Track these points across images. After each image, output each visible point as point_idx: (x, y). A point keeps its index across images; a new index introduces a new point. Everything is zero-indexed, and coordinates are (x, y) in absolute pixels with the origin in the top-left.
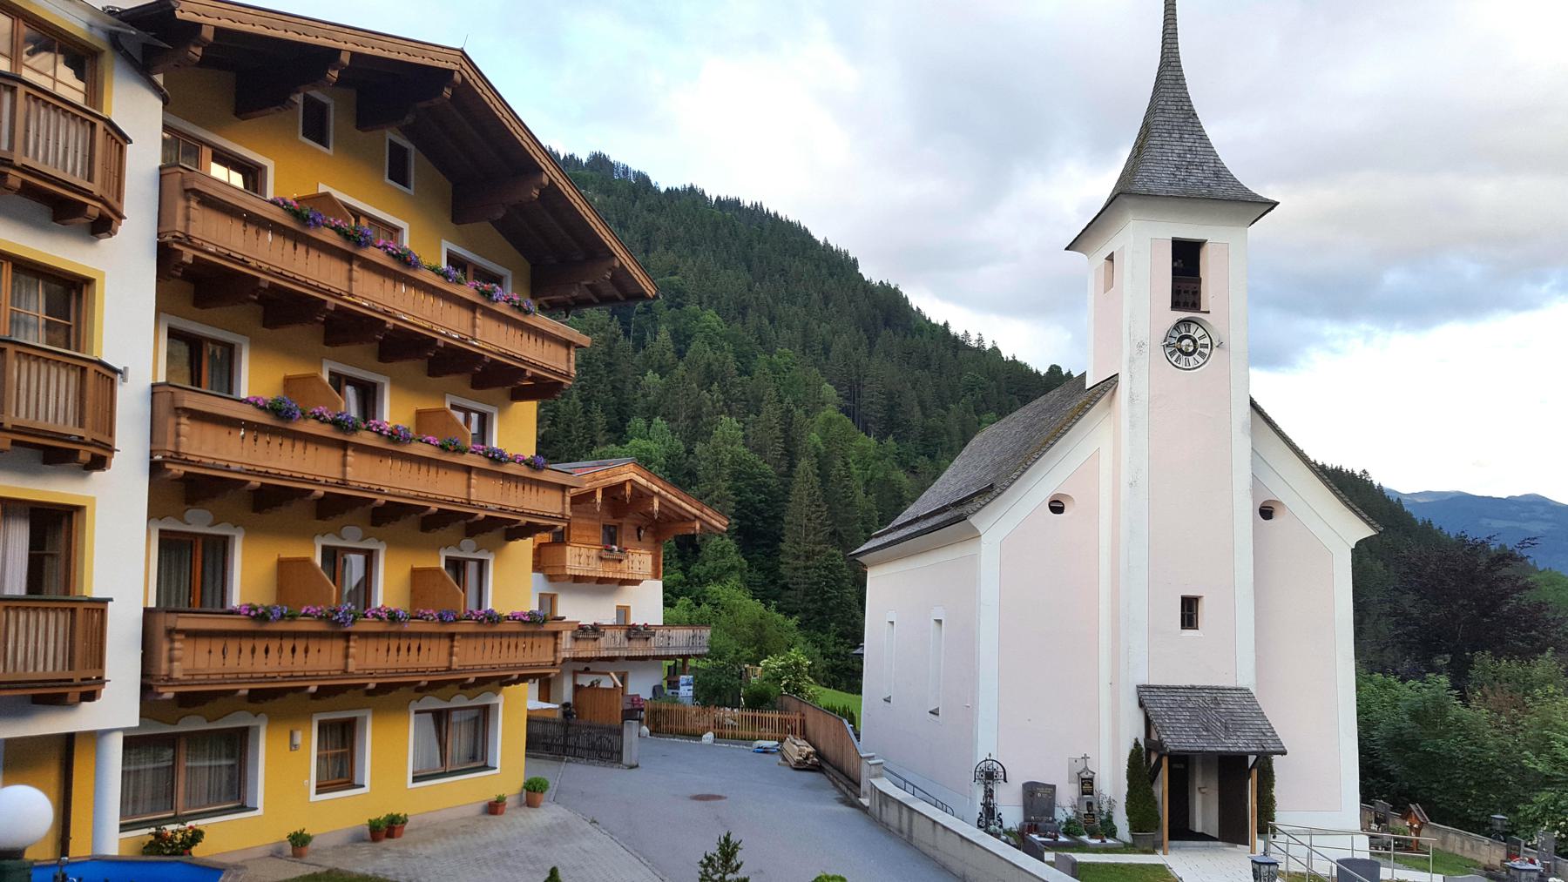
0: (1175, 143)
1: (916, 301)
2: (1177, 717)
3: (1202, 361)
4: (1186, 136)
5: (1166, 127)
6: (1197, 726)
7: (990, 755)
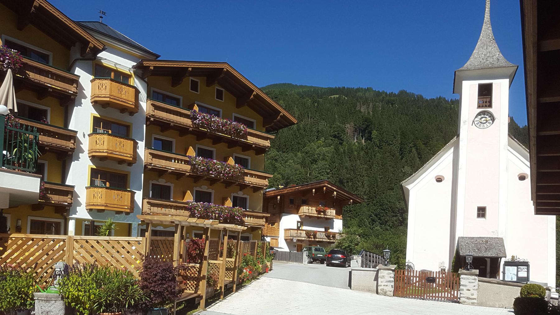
4: (489, 47)
7: (409, 261)
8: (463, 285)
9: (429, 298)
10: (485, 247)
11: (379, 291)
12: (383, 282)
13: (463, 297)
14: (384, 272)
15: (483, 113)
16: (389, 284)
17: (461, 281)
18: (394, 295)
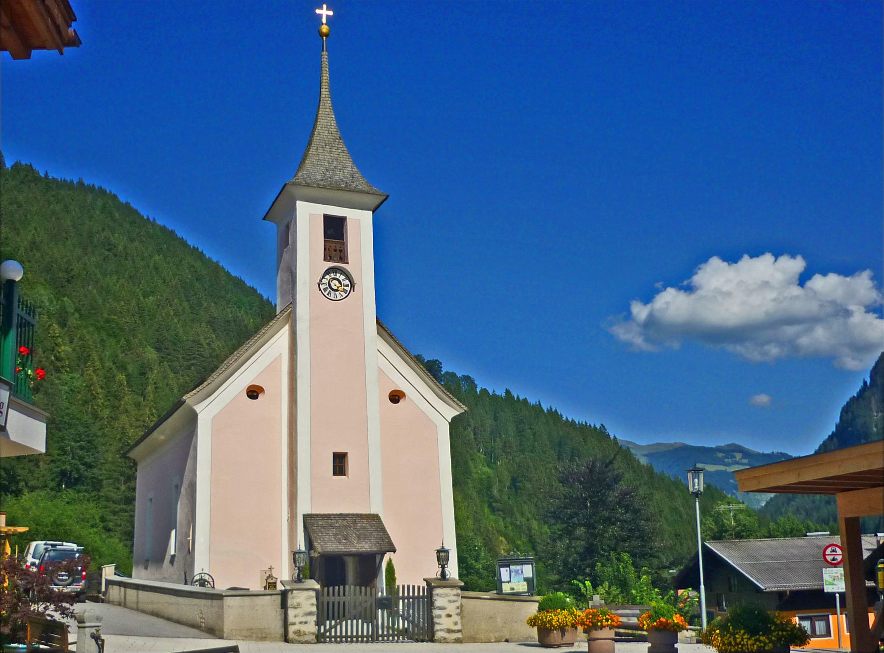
0: (327, 154)
1: (789, 454)
2: (327, 532)
3: (345, 295)
4: (335, 150)
5: (321, 144)
6: (340, 537)
7: (203, 570)
8: (440, 608)
9: (383, 640)
11: (291, 635)
12: (298, 616)
17: (435, 600)
18: (317, 640)
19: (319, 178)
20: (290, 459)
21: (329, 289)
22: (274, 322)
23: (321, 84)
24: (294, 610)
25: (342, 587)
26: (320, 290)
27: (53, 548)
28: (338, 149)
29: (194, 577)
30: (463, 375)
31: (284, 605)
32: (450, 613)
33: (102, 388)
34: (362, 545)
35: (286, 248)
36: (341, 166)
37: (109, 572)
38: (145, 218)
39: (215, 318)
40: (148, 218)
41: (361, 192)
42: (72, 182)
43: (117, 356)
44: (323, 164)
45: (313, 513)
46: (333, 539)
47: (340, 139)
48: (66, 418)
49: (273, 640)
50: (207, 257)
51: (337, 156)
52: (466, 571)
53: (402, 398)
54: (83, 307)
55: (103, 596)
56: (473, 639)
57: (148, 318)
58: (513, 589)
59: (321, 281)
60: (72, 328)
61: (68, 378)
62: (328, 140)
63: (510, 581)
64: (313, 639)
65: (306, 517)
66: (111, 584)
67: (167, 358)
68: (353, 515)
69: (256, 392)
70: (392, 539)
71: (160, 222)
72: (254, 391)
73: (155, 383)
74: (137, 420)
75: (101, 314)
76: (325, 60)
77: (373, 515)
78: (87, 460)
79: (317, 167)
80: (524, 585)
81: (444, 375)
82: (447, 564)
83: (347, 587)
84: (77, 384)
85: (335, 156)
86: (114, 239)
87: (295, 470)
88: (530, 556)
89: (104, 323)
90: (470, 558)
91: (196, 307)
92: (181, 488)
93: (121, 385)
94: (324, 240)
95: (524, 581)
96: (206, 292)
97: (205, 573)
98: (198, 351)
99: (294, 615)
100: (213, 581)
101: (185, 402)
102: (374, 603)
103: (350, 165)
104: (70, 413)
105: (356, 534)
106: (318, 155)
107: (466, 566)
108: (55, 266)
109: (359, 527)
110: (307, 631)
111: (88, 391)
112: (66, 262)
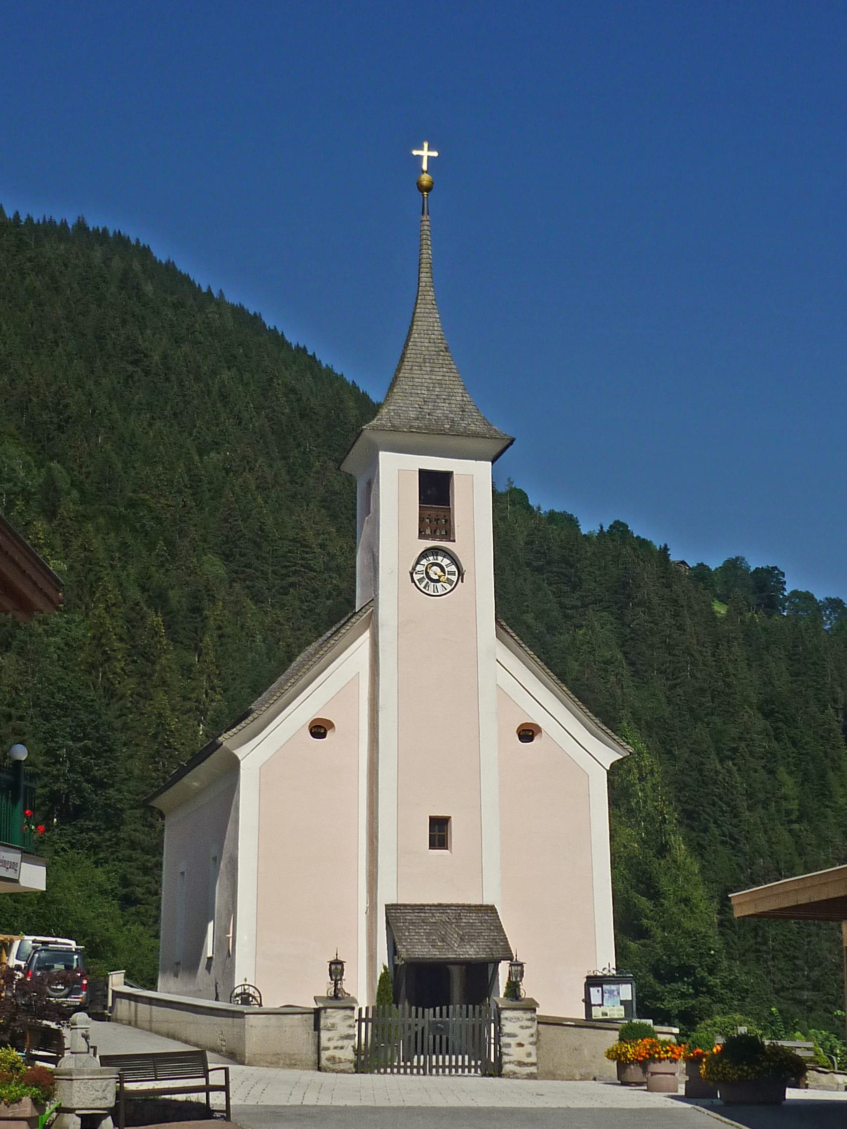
0: (427, 377)
3: (449, 588)
5: (418, 360)
7: (246, 980)
8: (509, 1035)
10: (458, 934)
11: (324, 1062)
13: (510, 1062)
14: (334, 1015)
15: (434, 551)
16: (345, 1043)
17: (504, 1025)
19: (412, 415)
20: (369, 824)
21: (427, 580)
22: (348, 628)
23: (420, 264)
24: (328, 1032)
25: (444, 1008)
26: (413, 581)
27: (44, 947)
28: (443, 367)
29: (235, 989)
30: (827, 599)
31: (317, 1027)
32: (522, 1042)
33: (121, 639)
34: (464, 950)
35: (367, 516)
36: (446, 393)
37: (117, 981)
38: (204, 290)
39: (336, 493)
40: (210, 292)
41: (475, 435)
42: (64, 224)
43: (149, 578)
44: (419, 392)
45: (399, 902)
46: (424, 941)
47: (447, 352)
48: (59, 697)
49: (305, 1067)
50: (324, 366)
51: (441, 378)
52: (693, 988)
53: (537, 735)
54: (87, 477)
55: (110, 1013)
56: (552, 1075)
57: (207, 495)
58: (606, 1015)
59: (414, 569)
60: (68, 520)
61: (62, 622)
62: (428, 353)
63: (602, 1005)
64: (350, 1068)
65: (388, 907)
66: (118, 997)
67: (243, 572)
68: (458, 906)
69: (323, 727)
70: (511, 946)
71: (232, 298)
72: (320, 727)
73: (220, 628)
74: (185, 698)
75: (121, 492)
76: (426, 228)
77: (487, 906)
78: (97, 773)
79: (411, 399)
80: (621, 1010)
81: (786, 599)
82: (521, 981)
83: (451, 1007)
84: (77, 632)
85: (438, 378)
86: (144, 341)
87: (375, 843)
88: (628, 973)
89: (126, 509)
90: (699, 969)
91: (301, 472)
92: (220, 863)
93: (156, 633)
94: (420, 507)
95: (621, 1004)
96: (320, 441)
97: (249, 985)
98: (303, 559)
99: (327, 1038)
100: (260, 997)
101: (222, 744)
102: (427, 1026)
103: (461, 391)
104: (66, 688)
105: (458, 934)
106: (413, 378)
107: (693, 981)
108: (35, 400)
109: (463, 924)
110: (343, 1058)
111: (97, 646)
112: (56, 393)
